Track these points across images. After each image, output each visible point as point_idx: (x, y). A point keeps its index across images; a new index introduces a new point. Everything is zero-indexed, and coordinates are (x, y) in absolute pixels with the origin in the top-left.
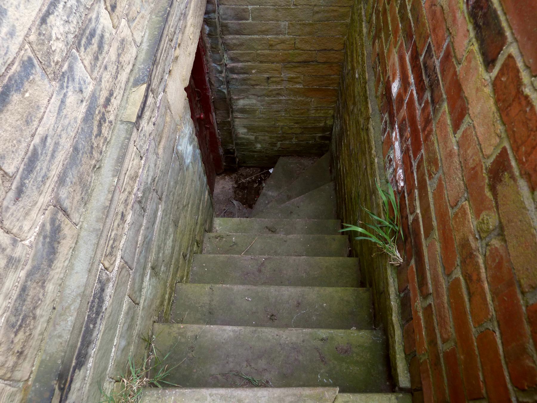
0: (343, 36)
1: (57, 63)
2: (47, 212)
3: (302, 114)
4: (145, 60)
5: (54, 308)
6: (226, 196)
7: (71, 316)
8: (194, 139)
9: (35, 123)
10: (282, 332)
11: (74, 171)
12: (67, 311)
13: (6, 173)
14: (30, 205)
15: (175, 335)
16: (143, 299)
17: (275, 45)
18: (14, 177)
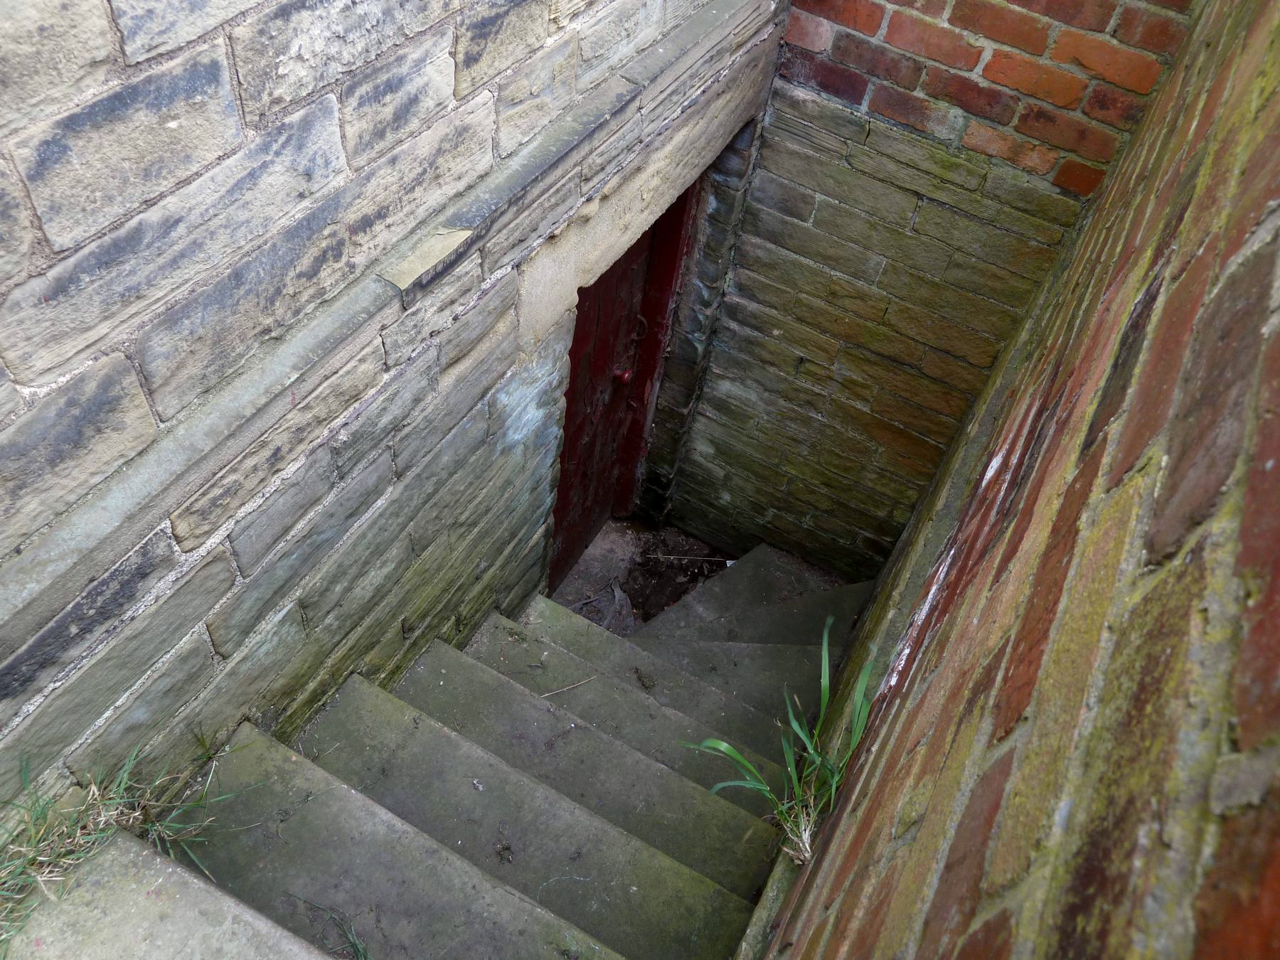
0: (998, 341)
1: (279, 100)
2: (104, 359)
3: (846, 469)
4: (498, 189)
5: (18, 551)
6: (608, 571)
7: (38, 582)
8: (556, 401)
9: (165, 183)
10: (488, 886)
11: (212, 317)
12: (37, 569)
13: (47, 240)
14: (72, 325)
15: (270, 769)
16: (242, 655)
17: (843, 297)
18: (62, 256)
